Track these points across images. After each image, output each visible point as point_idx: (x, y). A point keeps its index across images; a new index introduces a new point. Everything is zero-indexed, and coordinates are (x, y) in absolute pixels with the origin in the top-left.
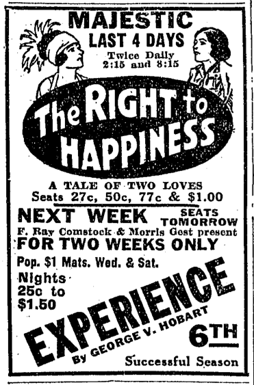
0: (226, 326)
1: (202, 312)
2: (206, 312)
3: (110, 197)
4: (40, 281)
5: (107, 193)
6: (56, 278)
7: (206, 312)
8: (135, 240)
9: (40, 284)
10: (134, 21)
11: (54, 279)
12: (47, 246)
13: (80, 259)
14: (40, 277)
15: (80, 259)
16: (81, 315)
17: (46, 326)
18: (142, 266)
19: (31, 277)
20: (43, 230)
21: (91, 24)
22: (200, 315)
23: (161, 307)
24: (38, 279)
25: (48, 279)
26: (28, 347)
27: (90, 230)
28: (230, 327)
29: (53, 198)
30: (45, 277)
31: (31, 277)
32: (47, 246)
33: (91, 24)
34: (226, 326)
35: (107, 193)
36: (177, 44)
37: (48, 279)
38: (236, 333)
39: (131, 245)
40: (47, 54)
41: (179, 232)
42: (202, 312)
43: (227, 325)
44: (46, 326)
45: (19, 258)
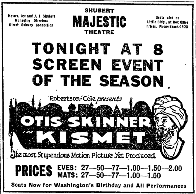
0: (118, 17)
1: (111, 11)
2: (112, 12)
3: (99, 175)
4: (79, 186)
5: (97, 173)
6: (107, 186)
7: (112, 12)
8: (82, 61)
9: (79, 188)
10: (70, 168)
11: (80, 186)
12: (61, 67)
13: (22, 183)
14: (79, 185)
15: (22, 183)
16: (20, 166)
17: (122, 60)
18: (14, 186)
19: (101, 185)
20: (24, 185)
21: (63, 176)
22: (109, 12)
23: (100, 24)
24: (78, 186)
25: (110, 186)
26: (89, 150)
27: (22, 184)
28: (91, 31)
29: (21, 185)
30: (109, 185)
31: (101, 185)
32: (61, 67)
33: (63, 176)
34: (90, 30)
35: (97, 173)
36: (72, 176)
37: (110, 186)
38: (129, 51)
39: (78, 65)
40: (171, 157)
41: (16, 185)
42: (111, 11)
43: (87, 26)
44: (122, 60)
45: (147, 184)
